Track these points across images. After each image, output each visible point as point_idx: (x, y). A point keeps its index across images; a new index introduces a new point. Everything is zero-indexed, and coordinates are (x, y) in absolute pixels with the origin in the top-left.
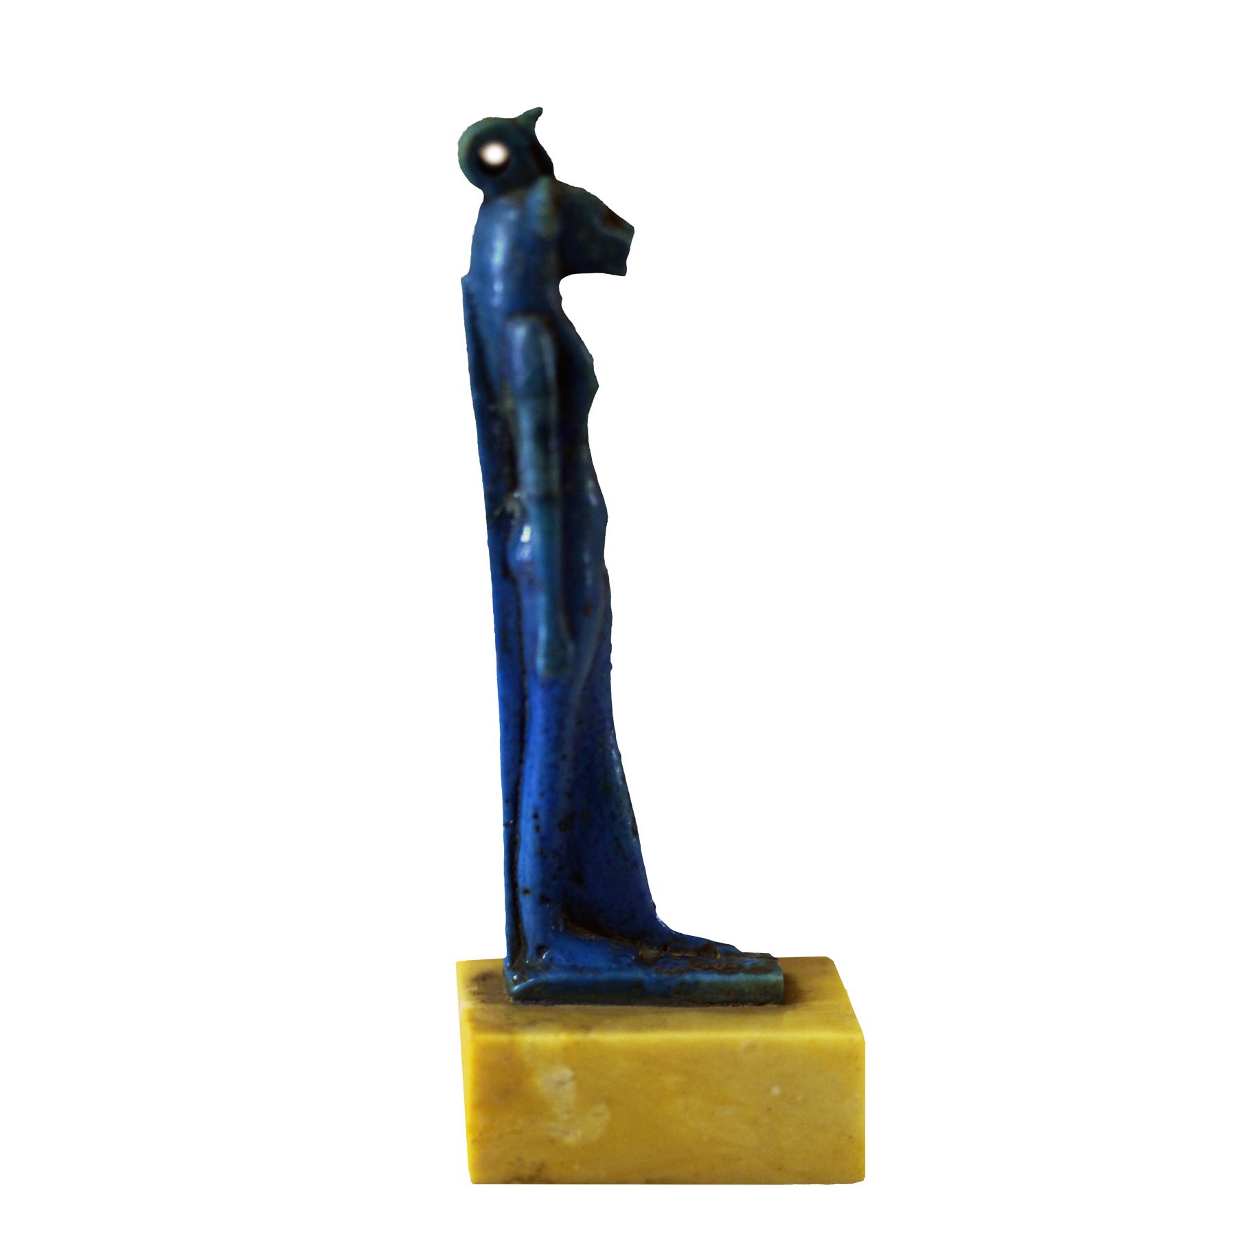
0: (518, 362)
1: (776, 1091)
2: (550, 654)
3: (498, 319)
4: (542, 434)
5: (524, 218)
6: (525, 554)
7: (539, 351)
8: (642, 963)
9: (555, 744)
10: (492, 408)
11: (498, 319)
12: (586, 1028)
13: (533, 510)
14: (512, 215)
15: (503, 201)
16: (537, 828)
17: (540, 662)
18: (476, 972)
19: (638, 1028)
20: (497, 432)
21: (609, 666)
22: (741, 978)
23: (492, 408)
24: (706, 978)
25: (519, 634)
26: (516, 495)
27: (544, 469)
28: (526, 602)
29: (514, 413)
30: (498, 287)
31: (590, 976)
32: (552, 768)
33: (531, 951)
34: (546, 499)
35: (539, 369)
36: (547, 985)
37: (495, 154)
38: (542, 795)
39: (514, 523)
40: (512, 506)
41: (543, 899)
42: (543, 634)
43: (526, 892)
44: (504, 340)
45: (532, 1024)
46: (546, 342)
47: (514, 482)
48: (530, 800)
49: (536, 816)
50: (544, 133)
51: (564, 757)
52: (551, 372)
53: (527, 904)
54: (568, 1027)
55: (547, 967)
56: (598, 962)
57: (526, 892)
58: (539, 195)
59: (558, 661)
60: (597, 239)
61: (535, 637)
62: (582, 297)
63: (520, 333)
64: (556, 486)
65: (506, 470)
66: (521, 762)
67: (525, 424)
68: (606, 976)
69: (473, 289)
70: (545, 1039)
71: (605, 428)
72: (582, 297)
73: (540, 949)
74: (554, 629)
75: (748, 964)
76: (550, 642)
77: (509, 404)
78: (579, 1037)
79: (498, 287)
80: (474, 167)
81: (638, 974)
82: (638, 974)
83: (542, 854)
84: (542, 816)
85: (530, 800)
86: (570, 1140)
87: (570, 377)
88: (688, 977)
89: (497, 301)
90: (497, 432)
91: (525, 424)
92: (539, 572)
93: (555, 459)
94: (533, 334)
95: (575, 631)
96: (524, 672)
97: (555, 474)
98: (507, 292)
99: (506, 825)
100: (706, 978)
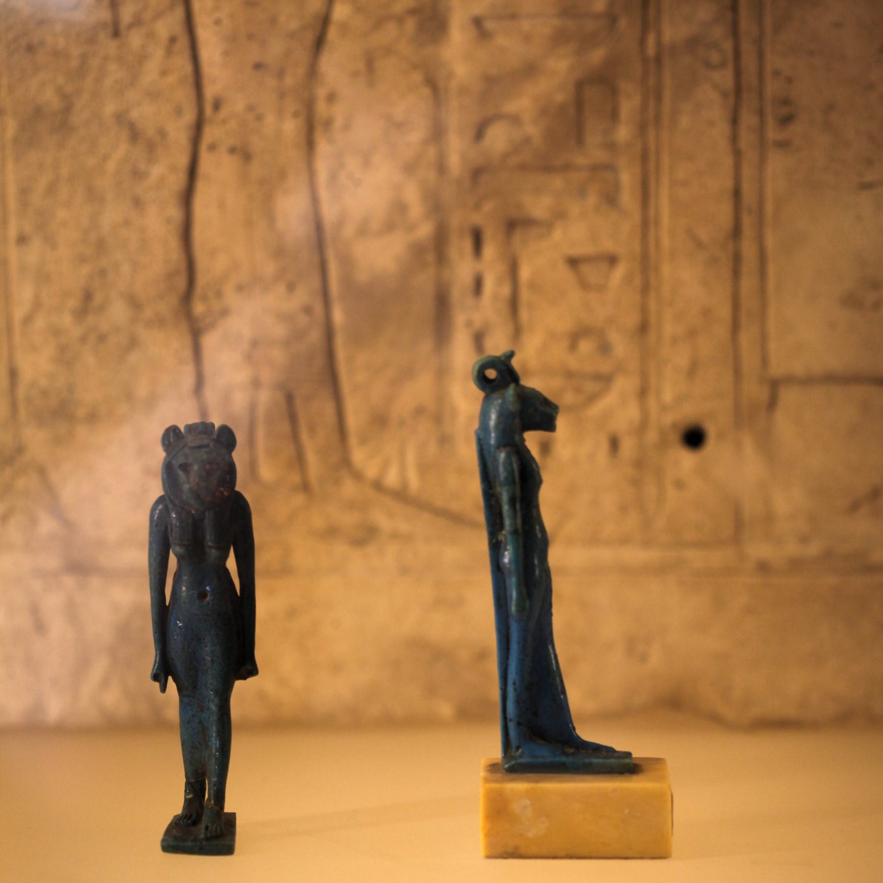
0: (501, 469)
1: (626, 811)
2: (518, 605)
3: (492, 450)
4: (512, 502)
5: (504, 403)
6: (506, 560)
7: (511, 464)
8: (565, 754)
9: (523, 650)
10: (491, 492)
11: (492, 450)
12: (537, 781)
13: (509, 538)
14: (500, 401)
15: (495, 396)
16: (515, 689)
17: (513, 609)
18: (491, 762)
19: (561, 782)
20: (493, 502)
21: (551, 615)
22: (612, 761)
23: (491, 492)
24: (595, 761)
25: (506, 598)
26: (504, 532)
27: (514, 518)
28: (508, 582)
29: (500, 494)
30: (493, 435)
31: (540, 760)
32: (521, 662)
33: (514, 749)
34: (515, 532)
35: (511, 472)
36: (521, 765)
37: (491, 374)
38: (517, 673)
39: (502, 546)
40: (501, 538)
41: (519, 724)
42: (514, 594)
43: (511, 720)
44: (496, 460)
45: (512, 780)
46: (514, 459)
47: (502, 527)
48: (512, 676)
49: (514, 684)
50: (515, 363)
51: (527, 656)
52: (517, 473)
53: (512, 726)
54: (528, 781)
55: (521, 756)
56: (545, 753)
57: (511, 720)
58: (511, 391)
59: (521, 609)
60: (537, 413)
61: (511, 597)
62: (532, 440)
63: (502, 456)
64: (519, 526)
65: (498, 521)
66: (508, 658)
67: (505, 498)
68: (549, 760)
69: (481, 437)
70: (518, 787)
71: (549, 498)
72: (532, 440)
73: (518, 748)
74: (520, 593)
75: (616, 755)
76: (518, 600)
77: (498, 489)
78: (533, 785)
79: (493, 435)
80: (482, 381)
81: (564, 759)
82: (564, 759)
83: (518, 702)
84: (517, 684)
85: (512, 676)
86: (530, 835)
87: (527, 478)
88: (587, 760)
89: (492, 442)
90: (493, 502)
91: (505, 498)
92: (513, 568)
93: (519, 514)
94: (508, 456)
95: (530, 595)
96: (508, 616)
97: (519, 521)
98: (497, 438)
99: (502, 689)
100: (595, 761)
